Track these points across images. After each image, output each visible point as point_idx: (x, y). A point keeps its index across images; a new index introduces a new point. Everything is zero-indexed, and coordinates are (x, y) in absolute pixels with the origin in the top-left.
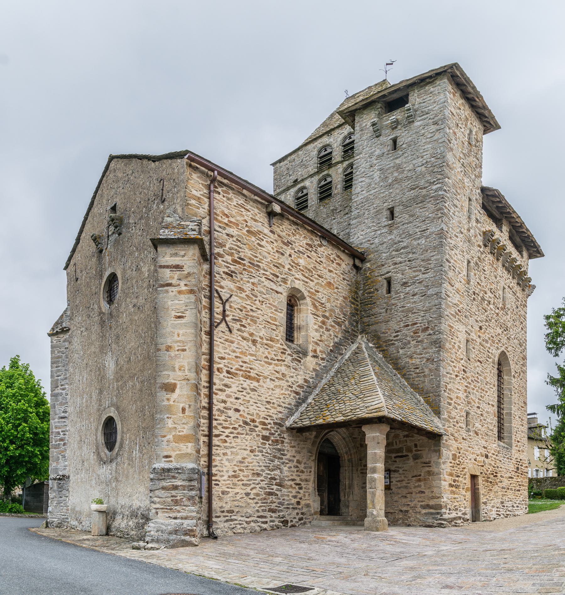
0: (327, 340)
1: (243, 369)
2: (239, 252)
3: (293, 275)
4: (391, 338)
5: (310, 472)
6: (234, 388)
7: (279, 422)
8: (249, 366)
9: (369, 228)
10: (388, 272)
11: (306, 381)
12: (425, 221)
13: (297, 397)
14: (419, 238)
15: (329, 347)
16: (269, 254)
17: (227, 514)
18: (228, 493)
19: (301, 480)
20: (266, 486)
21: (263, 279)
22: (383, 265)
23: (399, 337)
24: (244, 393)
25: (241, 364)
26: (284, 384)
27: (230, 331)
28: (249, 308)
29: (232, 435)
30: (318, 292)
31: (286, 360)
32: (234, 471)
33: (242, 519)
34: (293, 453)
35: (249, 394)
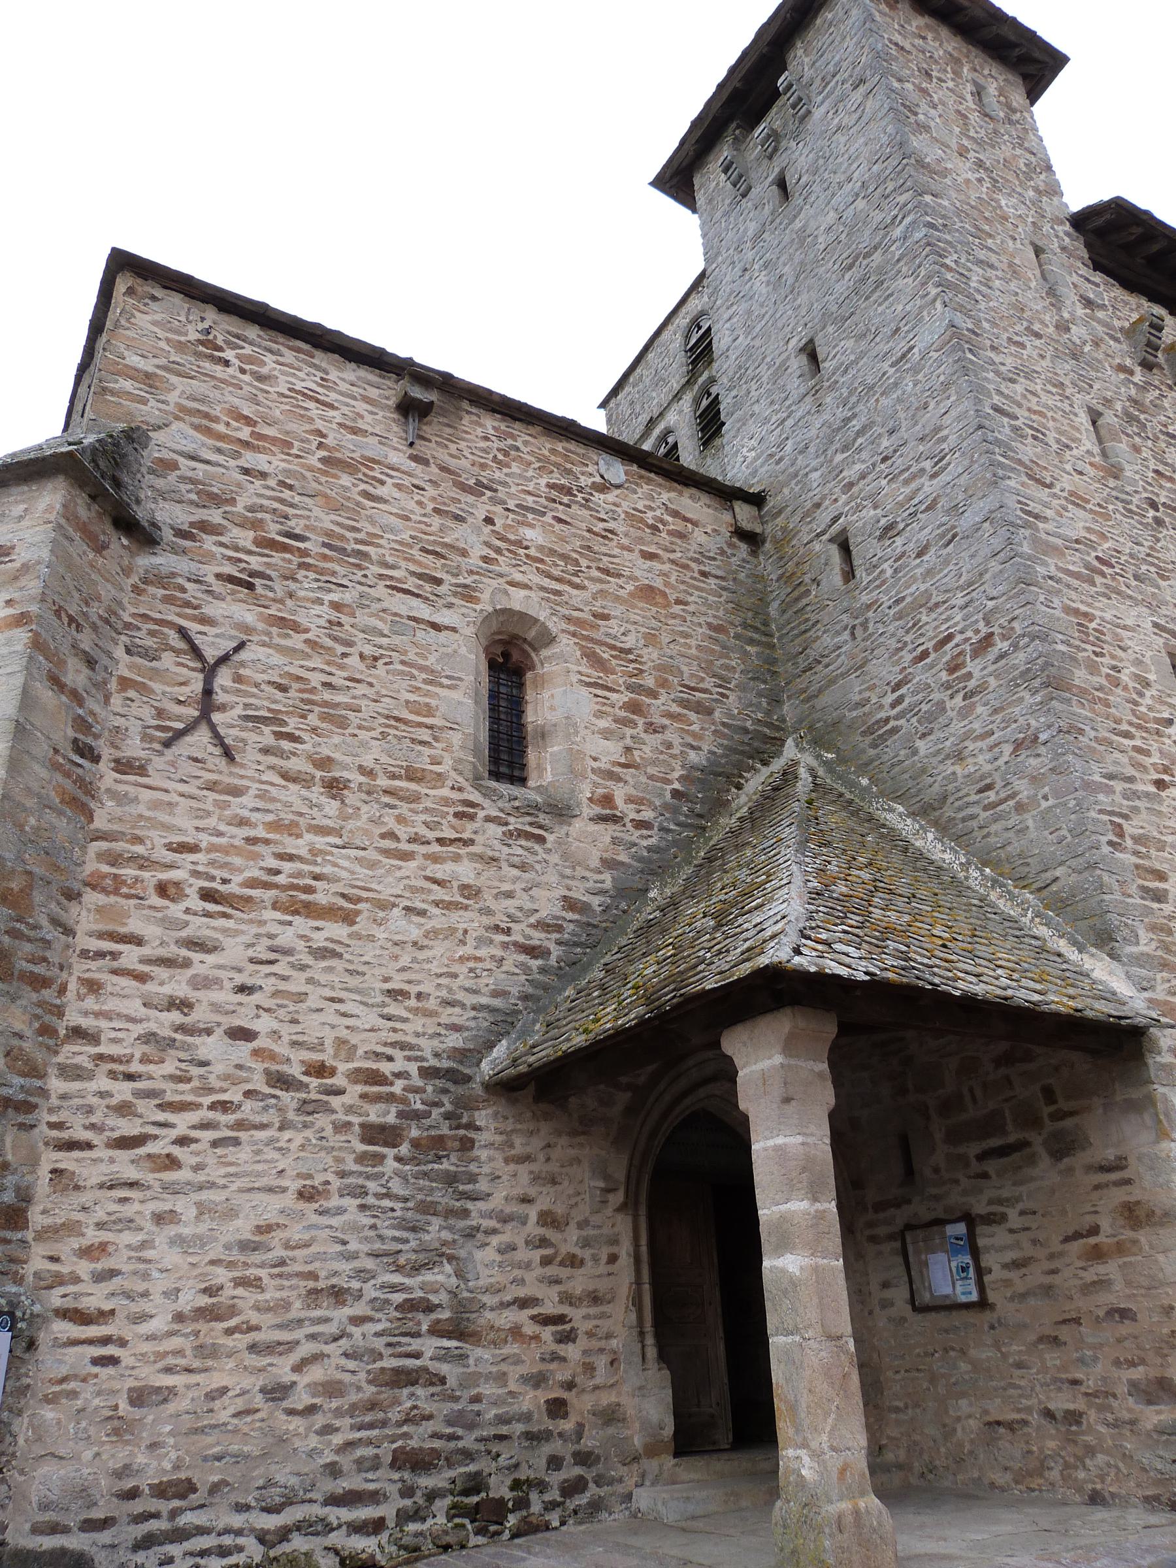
0: (654, 763)
1: (281, 879)
2: (286, 517)
3: (501, 575)
4: (882, 715)
5: (613, 1259)
6: (234, 951)
7: (445, 1064)
8: (306, 868)
9: (767, 420)
10: (835, 519)
11: (570, 904)
12: (898, 329)
13: (535, 963)
14: (896, 384)
15: (668, 782)
16: (408, 519)
17: (154, 1505)
18: (166, 1395)
19: (567, 1298)
20: (379, 1344)
21: (381, 591)
22: (818, 505)
23: (907, 701)
24: (280, 968)
25: (273, 863)
26: (470, 921)
27: (228, 754)
28: (316, 679)
29: (209, 1135)
30: (606, 617)
31: (479, 838)
32: (205, 1291)
33: (237, 1520)
34: (524, 1185)
35: (303, 968)
